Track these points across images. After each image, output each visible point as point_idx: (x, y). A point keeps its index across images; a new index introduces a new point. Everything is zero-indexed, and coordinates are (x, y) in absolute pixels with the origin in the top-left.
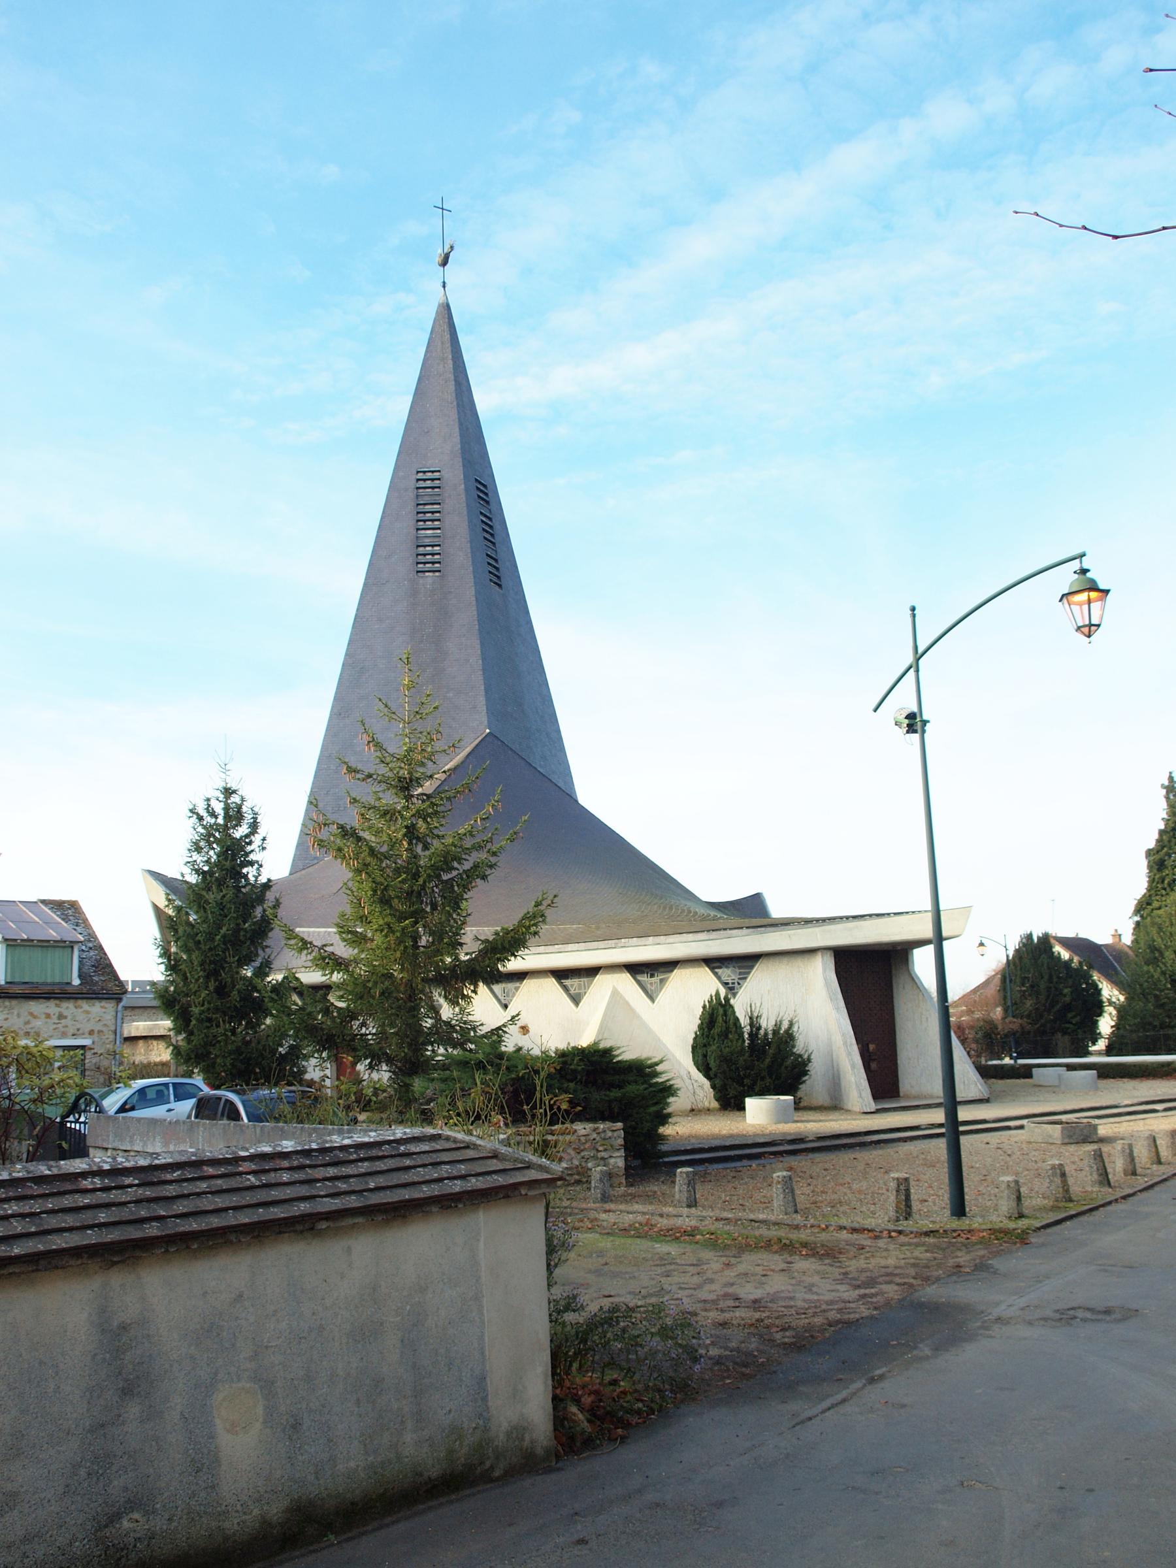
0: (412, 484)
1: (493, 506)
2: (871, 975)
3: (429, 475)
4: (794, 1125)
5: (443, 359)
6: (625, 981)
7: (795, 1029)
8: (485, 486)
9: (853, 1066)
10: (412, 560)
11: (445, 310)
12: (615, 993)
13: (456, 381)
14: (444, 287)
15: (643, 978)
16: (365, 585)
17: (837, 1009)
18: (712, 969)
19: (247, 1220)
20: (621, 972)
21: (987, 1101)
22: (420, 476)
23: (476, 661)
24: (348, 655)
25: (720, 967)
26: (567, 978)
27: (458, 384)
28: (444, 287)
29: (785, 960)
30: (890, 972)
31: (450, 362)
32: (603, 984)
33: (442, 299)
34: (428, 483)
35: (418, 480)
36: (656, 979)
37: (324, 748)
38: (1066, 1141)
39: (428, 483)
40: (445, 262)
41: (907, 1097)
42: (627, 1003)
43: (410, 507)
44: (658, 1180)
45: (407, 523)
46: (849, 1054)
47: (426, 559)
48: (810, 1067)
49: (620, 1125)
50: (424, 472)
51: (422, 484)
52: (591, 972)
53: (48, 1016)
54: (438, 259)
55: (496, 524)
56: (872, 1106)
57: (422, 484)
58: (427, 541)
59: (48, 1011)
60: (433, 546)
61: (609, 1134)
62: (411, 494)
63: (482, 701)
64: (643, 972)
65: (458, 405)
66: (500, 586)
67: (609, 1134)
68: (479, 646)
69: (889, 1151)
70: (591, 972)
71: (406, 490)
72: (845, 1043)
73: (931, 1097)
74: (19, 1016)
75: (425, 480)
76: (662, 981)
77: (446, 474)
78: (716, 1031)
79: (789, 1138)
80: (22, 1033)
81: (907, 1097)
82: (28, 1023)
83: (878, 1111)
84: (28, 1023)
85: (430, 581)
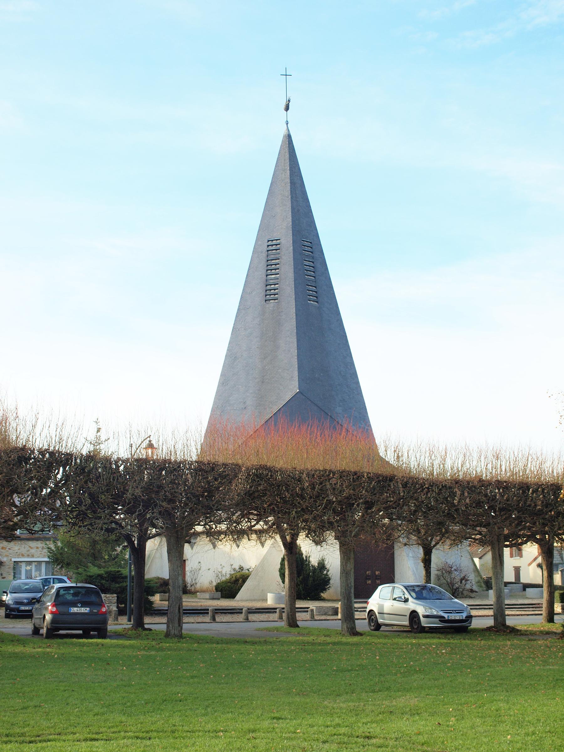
0: (265, 248)
5: (284, 170)
10: (264, 293)
11: (289, 138)
14: (287, 124)
16: (239, 310)
19: (74, 639)
22: (270, 243)
24: (229, 350)
27: (292, 183)
28: (287, 124)
31: (288, 172)
35: (268, 246)
40: (287, 108)
43: (263, 264)
45: (262, 272)
47: (270, 293)
48: (331, 582)
49: (115, 595)
50: (272, 240)
51: (270, 248)
53: (37, 548)
54: (283, 106)
57: (270, 248)
59: (37, 546)
61: (111, 598)
62: (265, 255)
63: (296, 374)
67: (111, 598)
68: (296, 343)
71: (262, 252)
74: (24, 548)
75: (272, 245)
77: (283, 241)
80: (26, 555)
82: (29, 551)
84: (29, 551)
85: (272, 305)
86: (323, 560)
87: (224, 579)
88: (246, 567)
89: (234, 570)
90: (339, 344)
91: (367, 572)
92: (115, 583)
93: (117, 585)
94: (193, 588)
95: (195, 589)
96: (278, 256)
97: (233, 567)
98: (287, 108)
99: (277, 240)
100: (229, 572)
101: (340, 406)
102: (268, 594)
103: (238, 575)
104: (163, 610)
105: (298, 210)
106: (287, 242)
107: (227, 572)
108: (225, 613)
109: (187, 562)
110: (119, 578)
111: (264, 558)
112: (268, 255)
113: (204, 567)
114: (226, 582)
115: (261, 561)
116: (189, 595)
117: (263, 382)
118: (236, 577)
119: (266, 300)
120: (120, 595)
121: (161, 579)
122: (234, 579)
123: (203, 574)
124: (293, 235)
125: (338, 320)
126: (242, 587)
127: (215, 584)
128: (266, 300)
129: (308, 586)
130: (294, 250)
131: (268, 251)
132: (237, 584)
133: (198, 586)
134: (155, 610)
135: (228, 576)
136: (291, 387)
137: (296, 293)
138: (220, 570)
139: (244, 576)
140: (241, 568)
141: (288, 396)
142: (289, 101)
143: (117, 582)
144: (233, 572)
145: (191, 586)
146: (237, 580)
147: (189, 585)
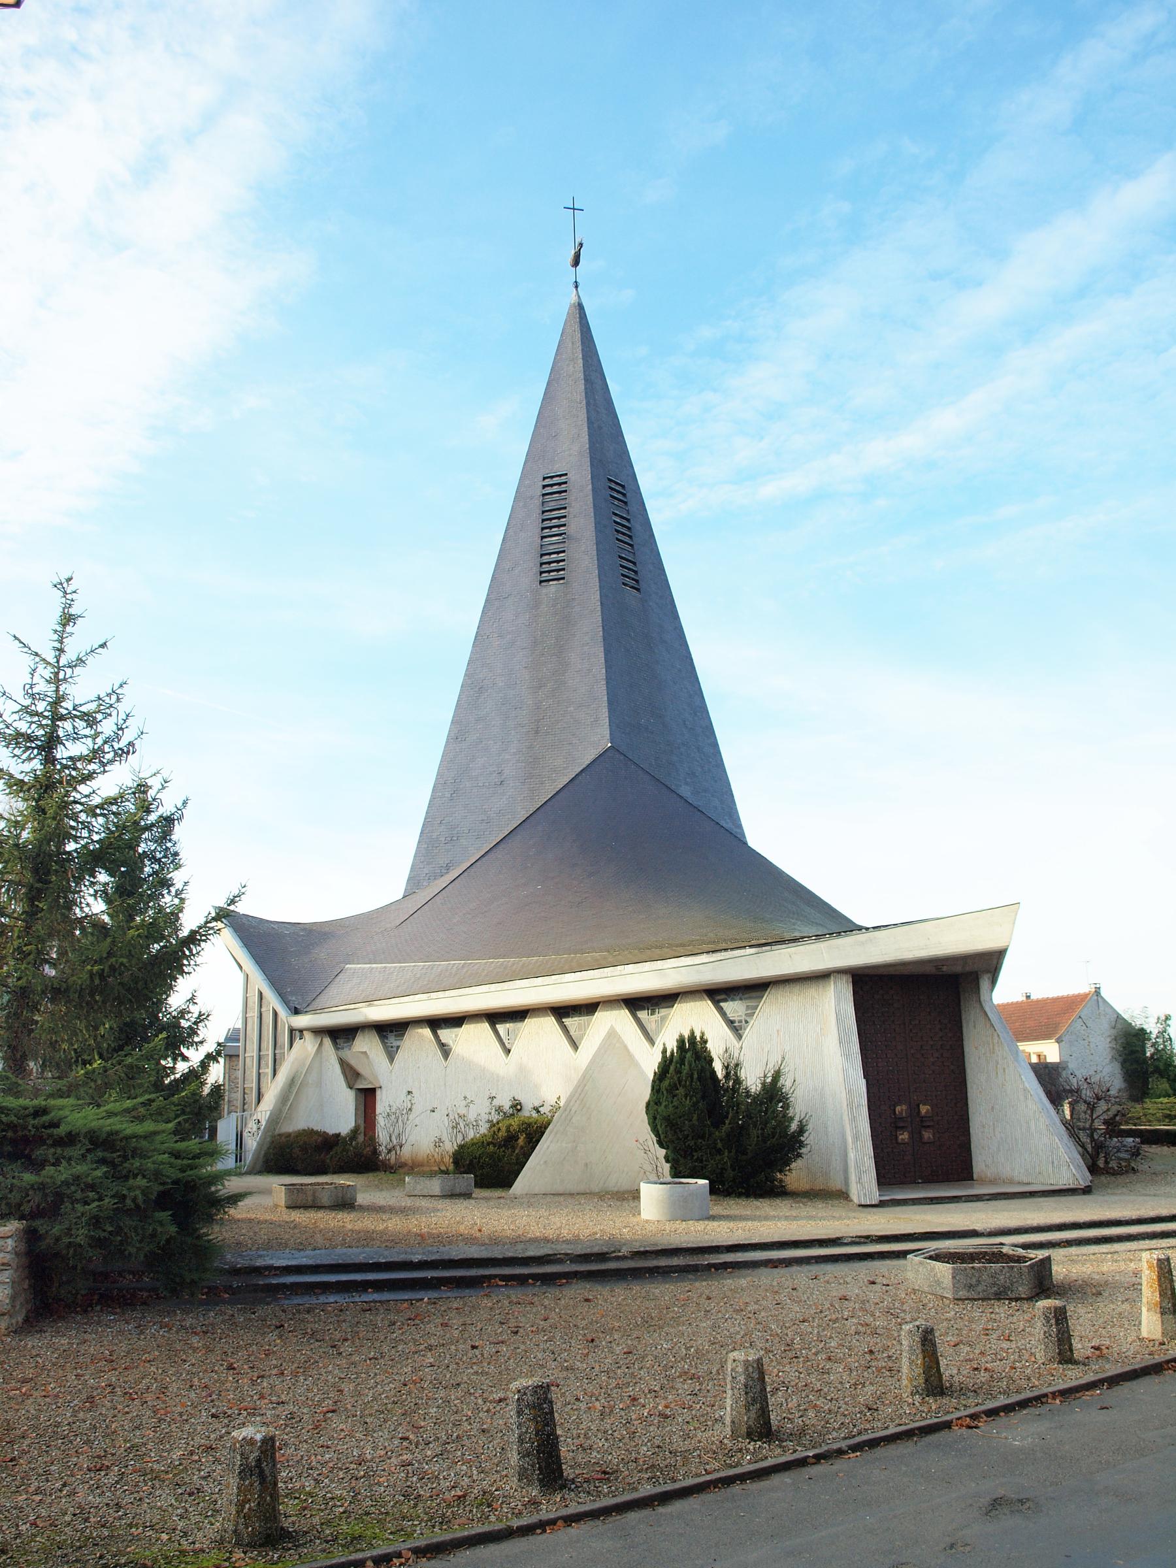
0: (539, 491)
1: (633, 507)
2: (920, 1011)
3: (556, 480)
4: (700, 1226)
6: (621, 1018)
7: (781, 1081)
8: (623, 487)
9: (856, 1137)
10: (537, 569)
12: (612, 1034)
13: (586, 380)
14: (576, 287)
15: (643, 1015)
17: (847, 1056)
18: (716, 1003)
20: (620, 1008)
21: (1087, 1191)
22: (548, 482)
23: (600, 671)
24: (468, 675)
25: (725, 1000)
26: (567, 1015)
28: (576, 287)
29: (796, 988)
30: (959, 1005)
31: (580, 362)
32: (604, 1020)
33: (573, 299)
34: (556, 489)
35: (544, 487)
36: (656, 1017)
37: (440, 775)
38: (962, 1294)
39: (556, 489)
40: (576, 262)
41: (983, 1182)
42: (626, 1047)
43: (536, 516)
44: (554, 1284)
46: (854, 1119)
47: (551, 568)
50: (552, 477)
51: (549, 490)
52: (588, 1008)
55: (636, 526)
56: (875, 1196)
57: (549, 490)
58: (552, 548)
60: (558, 553)
64: (643, 1008)
65: (588, 404)
66: (638, 590)
68: (602, 655)
69: (743, 1281)
70: (588, 1008)
72: (850, 1105)
73: (1011, 1182)
76: (664, 1019)
77: (572, 477)
78: (666, 1083)
79: (579, 1250)
81: (983, 1182)
83: (882, 1204)
86: (777, 1075)
87: (471, 1135)
88: (529, 1103)
89: (499, 1109)
90: (680, 670)
91: (898, 1109)
92: (26, 1169)
93: (29, 1177)
94: (392, 1156)
95: (398, 1157)
96: (563, 502)
97: (496, 1102)
98: (576, 262)
99: (560, 476)
100: (486, 1117)
101: (687, 784)
102: (642, 1184)
103: (515, 1123)
104: (270, 1268)
105: (600, 428)
106: (581, 480)
107: (479, 1119)
108: (522, 1280)
109: (378, 1092)
110: (41, 1141)
111: (584, 1076)
112: (546, 500)
113: (421, 1104)
114: (480, 1144)
115: (577, 1087)
116: (381, 1175)
117: (537, 732)
118: (508, 1130)
119: (541, 582)
120: (41, 1225)
121: (317, 1133)
122: (503, 1134)
123: (417, 1121)
124: (592, 465)
125: (675, 629)
126: (527, 1156)
127: (450, 1147)
128: (541, 582)
129: (744, 1153)
130: (594, 489)
131: (544, 495)
132: (514, 1148)
133: (406, 1153)
134: (236, 1272)
135: (484, 1129)
136: (595, 738)
137: (600, 567)
138: (462, 1111)
139: (529, 1125)
140: (517, 1106)
141: (589, 756)
142: (581, 245)
143: (37, 1166)
144: (495, 1118)
145: (390, 1151)
146: (511, 1138)
147: (383, 1149)
